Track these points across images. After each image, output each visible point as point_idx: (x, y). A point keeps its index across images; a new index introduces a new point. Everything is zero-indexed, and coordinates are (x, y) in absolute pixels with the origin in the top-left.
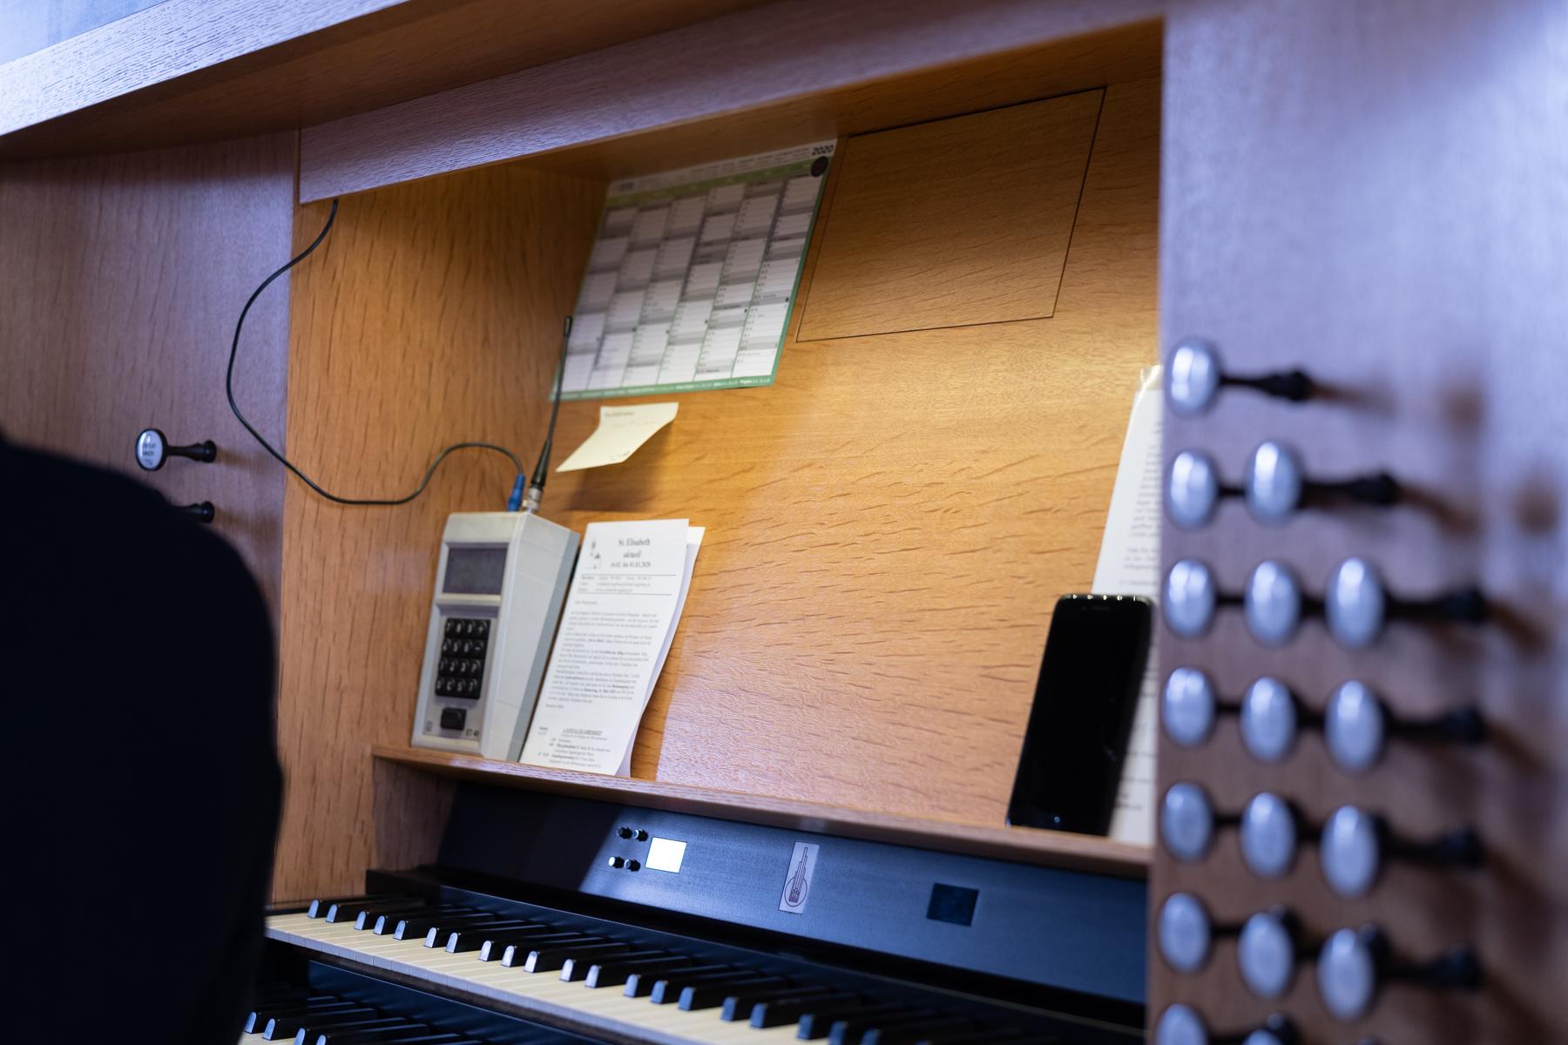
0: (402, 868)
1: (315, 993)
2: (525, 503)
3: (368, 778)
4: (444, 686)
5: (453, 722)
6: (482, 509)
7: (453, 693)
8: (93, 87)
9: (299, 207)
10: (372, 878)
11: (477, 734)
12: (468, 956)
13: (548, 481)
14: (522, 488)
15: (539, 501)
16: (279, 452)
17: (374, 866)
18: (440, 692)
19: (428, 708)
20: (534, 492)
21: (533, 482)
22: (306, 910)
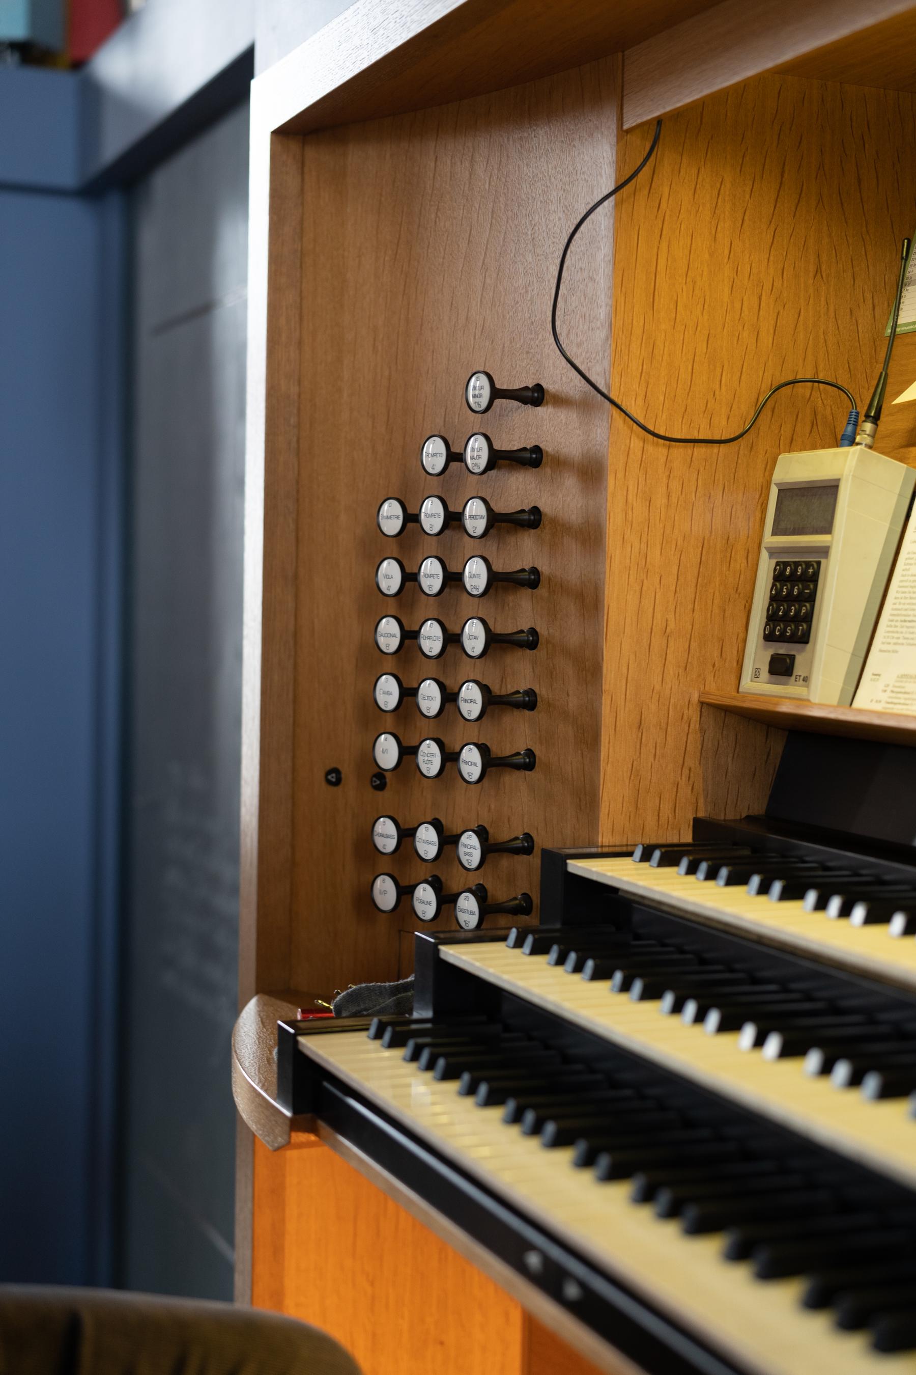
0: (730, 816)
1: (637, 937)
2: (858, 439)
3: (695, 725)
4: (772, 632)
5: (782, 668)
6: (814, 447)
7: (782, 639)
8: (415, 17)
9: (623, 134)
10: (699, 825)
11: (806, 679)
12: (792, 907)
13: (883, 417)
14: (856, 424)
15: (873, 436)
16: (604, 390)
17: (701, 814)
18: (769, 638)
19: (757, 654)
20: (868, 426)
21: (867, 416)
22: (630, 854)
